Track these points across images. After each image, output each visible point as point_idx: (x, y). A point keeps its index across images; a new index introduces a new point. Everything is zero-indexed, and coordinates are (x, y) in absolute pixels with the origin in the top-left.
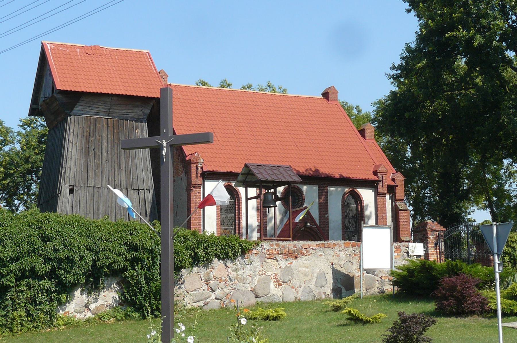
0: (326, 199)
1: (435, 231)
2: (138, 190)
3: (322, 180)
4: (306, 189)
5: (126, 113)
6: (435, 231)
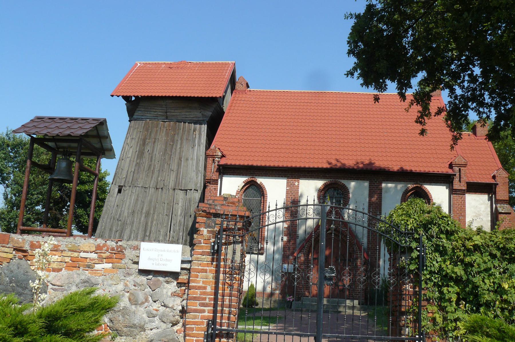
0: (380, 198)
1: (216, 215)
2: (186, 190)
3: (374, 175)
4: (355, 188)
5: (184, 116)
6: (216, 215)
